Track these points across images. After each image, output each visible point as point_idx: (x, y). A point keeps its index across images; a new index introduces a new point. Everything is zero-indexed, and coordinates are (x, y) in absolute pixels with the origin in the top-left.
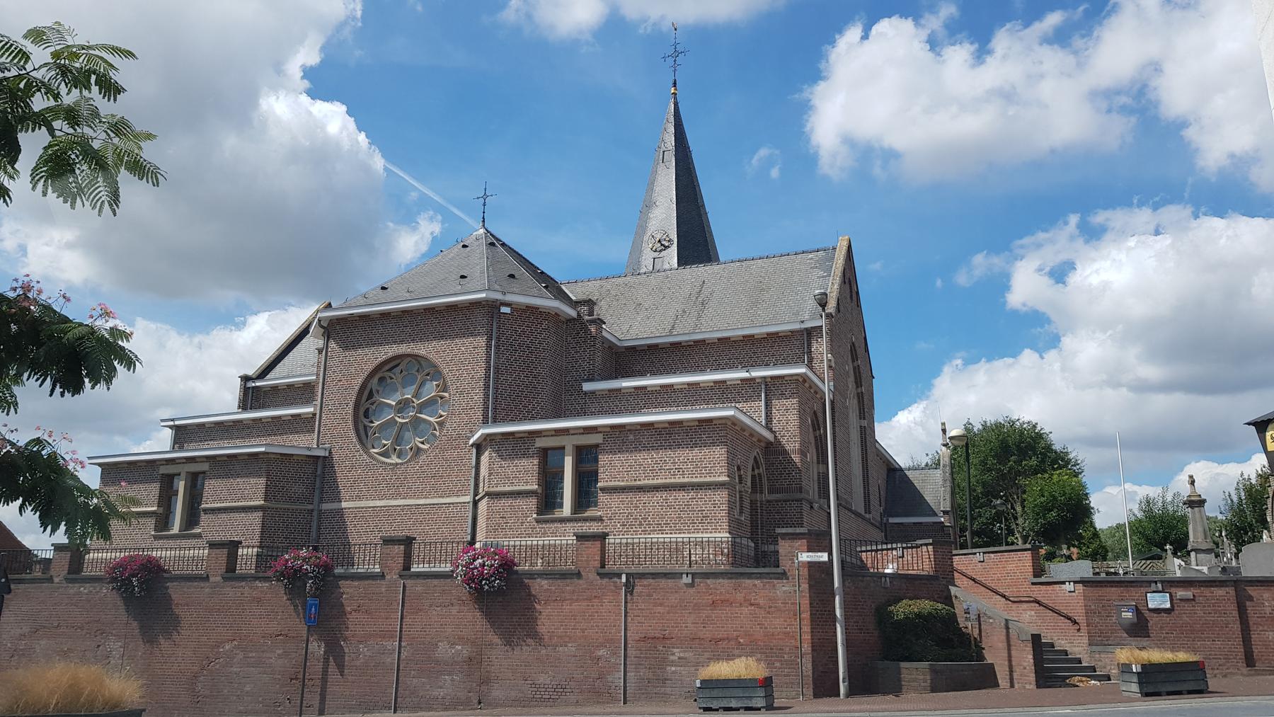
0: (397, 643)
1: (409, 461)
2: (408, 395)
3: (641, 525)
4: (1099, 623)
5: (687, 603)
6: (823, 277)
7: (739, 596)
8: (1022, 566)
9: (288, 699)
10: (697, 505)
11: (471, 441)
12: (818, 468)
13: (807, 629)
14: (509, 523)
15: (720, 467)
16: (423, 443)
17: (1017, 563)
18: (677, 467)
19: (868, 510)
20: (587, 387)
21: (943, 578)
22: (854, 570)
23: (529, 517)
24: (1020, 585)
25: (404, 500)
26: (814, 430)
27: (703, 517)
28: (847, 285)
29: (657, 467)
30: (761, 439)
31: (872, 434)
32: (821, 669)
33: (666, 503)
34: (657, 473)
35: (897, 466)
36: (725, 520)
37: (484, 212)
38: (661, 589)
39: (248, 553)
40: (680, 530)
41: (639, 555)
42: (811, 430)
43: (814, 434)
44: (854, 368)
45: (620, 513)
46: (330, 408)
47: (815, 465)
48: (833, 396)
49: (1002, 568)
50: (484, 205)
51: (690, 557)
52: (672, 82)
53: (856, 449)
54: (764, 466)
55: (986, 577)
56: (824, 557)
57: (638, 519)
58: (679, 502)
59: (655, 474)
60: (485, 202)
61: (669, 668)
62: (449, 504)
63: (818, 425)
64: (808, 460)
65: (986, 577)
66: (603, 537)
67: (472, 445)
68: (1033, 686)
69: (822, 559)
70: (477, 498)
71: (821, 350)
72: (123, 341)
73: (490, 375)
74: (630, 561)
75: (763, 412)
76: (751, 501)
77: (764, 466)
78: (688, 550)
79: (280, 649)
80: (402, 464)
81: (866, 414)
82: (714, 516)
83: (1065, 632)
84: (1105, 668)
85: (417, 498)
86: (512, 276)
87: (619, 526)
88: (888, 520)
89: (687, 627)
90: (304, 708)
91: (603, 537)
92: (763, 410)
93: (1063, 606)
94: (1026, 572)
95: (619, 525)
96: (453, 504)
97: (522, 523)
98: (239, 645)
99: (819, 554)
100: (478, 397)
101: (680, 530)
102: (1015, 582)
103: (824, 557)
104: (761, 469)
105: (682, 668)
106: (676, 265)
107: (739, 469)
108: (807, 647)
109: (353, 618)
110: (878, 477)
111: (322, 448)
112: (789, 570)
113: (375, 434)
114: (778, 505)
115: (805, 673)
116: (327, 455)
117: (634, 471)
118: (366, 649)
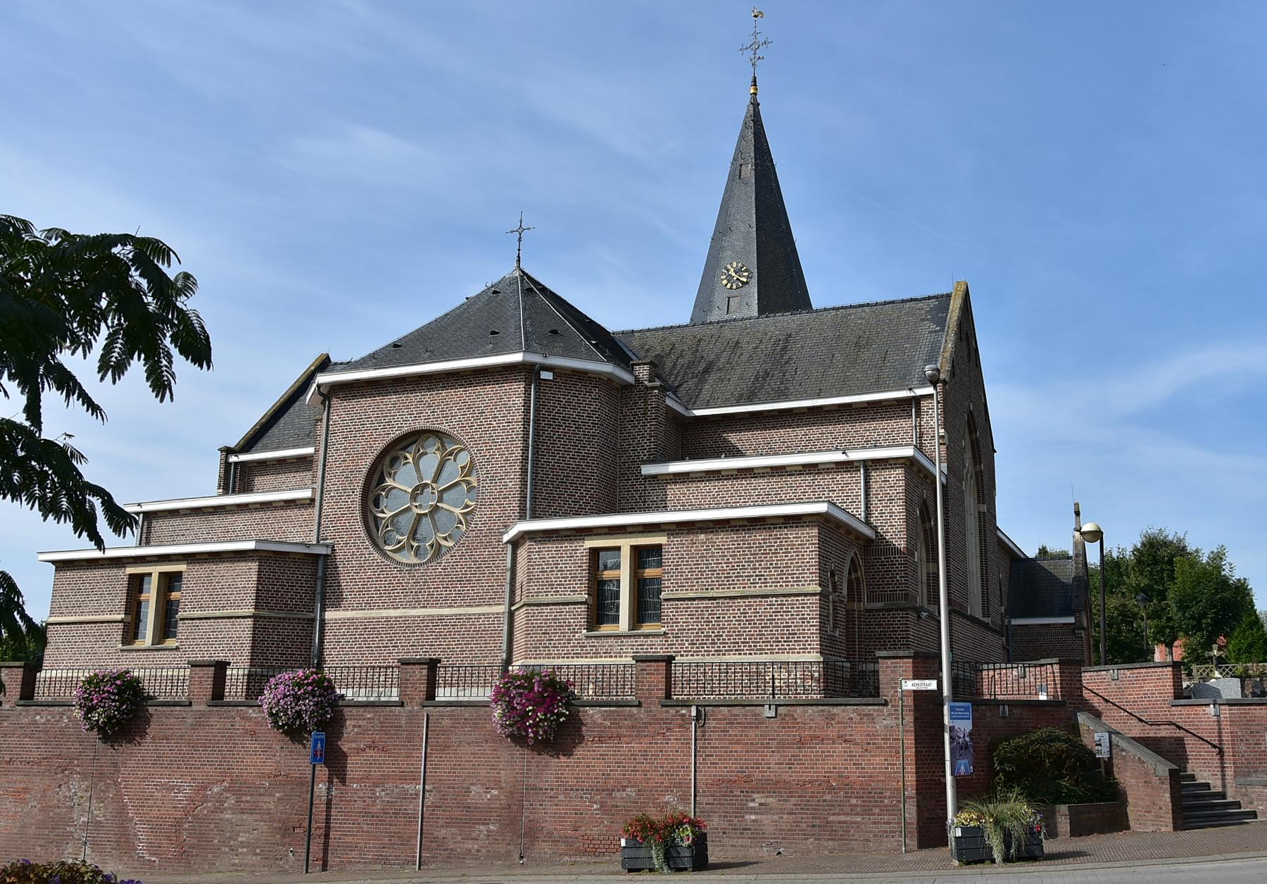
0: (421, 786)
1: (430, 561)
2: (426, 480)
3: (715, 643)
4: (1247, 752)
5: (770, 740)
6: (935, 331)
7: (832, 732)
8: (1162, 686)
9: (291, 851)
10: (782, 619)
11: (506, 538)
12: (927, 568)
13: (911, 768)
14: (552, 640)
15: (810, 573)
16: (445, 539)
17: (1156, 683)
18: (757, 573)
19: (986, 612)
20: (648, 470)
21: (1070, 703)
22: (965, 687)
23: (577, 633)
24: (1159, 708)
25: (423, 610)
26: (923, 522)
27: (789, 634)
28: (964, 341)
29: (734, 573)
30: (859, 536)
31: (993, 503)
32: (926, 815)
33: (745, 617)
34: (733, 580)
35: (1022, 556)
36: (816, 638)
37: (519, 250)
38: (738, 723)
39: (237, 673)
40: (761, 650)
41: (712, 680)
42: (919, 522)
43: (923, 527)
44: (972, 442)
45: (688, 630)
46: (332, 494)
47: (924, 564)
48: (947, 479)
49: (1139, 687)
50: (520, 240)
51: (773, 683)
52: (751, 79)
53: (973, 540)
54: (863, 568)
55: (1120, 698)
56: (932, 685)
57: (711, 636)
58: (760, 616)
59: (730, 582)
60: (520, 238)
61: (747, 817)
62: (479, 614)
63: (928, 515)
64: (916, 560)
65: (1120, 698)
66: (669, 660)
67: (506, 543)
68: (1170, 828)
69: (929, 688)
70: (513, 608)
71: (932, 423)
72: (163, 263)
73: (528, 457)
74: (701, 687)
75: (862, 503)
76: (847, 611)
77: (863, 568)
78: (771, 674)
79: (279, 792)
80: (420, 565)
81: (986, 497)
82: (802, 634)
83: (1209, 763)
84: (1251, 803)
85: (440, 607)
86: (554, 332)
87: (687, 645)
88: (1010, 622)
89: (770, 768)
90: (310, 862)
91: (669, 660)
92: (862, 500)
93: (1206, 733)
94: (1166, 693)
95: (687, 643)
96: (484, 615)
97: (569, 640)
98: (229, 787)
99: (927, 682)
100: (513, 483)
101: (761, 650)
102: (1153, 704)
103: (932, 685)
104: (859, 572)
105: (763, 817)
106: (756, 314)
107: (833, 574)
108: (911, 791)
109: (368, 756)
110: (1000, 573)
111: (323, 545)
112: (891, 700)
113: (387, 527)
114: (879, 615)
115: (907, 820)
116: (329, 552)
117: (705, 578)
118: (384, 793)
